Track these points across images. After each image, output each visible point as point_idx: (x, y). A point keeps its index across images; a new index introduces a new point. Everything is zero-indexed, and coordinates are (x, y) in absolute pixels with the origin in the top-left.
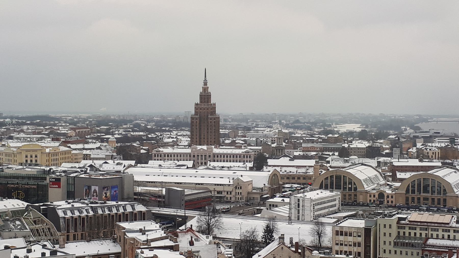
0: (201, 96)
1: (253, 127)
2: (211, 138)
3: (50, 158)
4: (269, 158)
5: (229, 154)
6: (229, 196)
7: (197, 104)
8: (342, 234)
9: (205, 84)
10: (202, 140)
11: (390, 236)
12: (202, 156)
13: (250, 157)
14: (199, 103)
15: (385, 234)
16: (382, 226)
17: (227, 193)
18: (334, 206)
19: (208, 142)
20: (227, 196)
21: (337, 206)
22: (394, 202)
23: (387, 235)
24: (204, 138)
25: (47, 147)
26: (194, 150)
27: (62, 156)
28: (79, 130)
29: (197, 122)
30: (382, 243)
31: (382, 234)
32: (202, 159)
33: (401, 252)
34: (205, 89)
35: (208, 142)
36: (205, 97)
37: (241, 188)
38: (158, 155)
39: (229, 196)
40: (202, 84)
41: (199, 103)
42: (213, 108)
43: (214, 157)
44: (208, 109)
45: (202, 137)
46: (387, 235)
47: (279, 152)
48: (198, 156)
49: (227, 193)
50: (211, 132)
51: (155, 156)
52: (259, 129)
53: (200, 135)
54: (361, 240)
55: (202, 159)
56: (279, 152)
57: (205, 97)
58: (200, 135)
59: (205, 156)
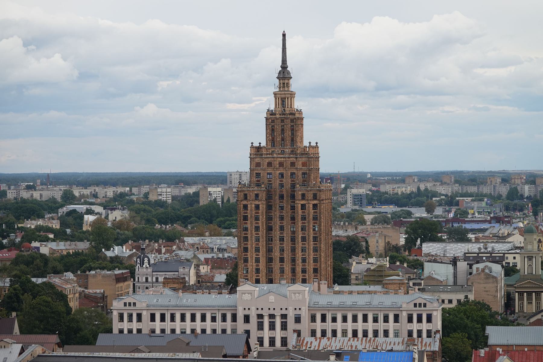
1: (447, 221)
2: (304, 260)
4: (491, 311)
7: (259, 148)
9: (284, 61)
10: (276, 265)
12: (272, 316)
13: (429, 320)
14: (264, 144)
19: (293, 271)
24: (282, 260)
29: (257, 207)
32: (272, 327)
35: (293, 271)
36: (284, 123)
38: (130, 316)
40: (274, 85)
41: (264, 144)
42: (311, 156)
43: (313, 319)
45: (276, 254)
47: (530, 303)
48: (260, 316)
52: (468, 226)
53: (269, 250)
55: (272, 327)
56: (530, 303)
57: (284, 123)
58: (269, 250)
59: (284, 316)
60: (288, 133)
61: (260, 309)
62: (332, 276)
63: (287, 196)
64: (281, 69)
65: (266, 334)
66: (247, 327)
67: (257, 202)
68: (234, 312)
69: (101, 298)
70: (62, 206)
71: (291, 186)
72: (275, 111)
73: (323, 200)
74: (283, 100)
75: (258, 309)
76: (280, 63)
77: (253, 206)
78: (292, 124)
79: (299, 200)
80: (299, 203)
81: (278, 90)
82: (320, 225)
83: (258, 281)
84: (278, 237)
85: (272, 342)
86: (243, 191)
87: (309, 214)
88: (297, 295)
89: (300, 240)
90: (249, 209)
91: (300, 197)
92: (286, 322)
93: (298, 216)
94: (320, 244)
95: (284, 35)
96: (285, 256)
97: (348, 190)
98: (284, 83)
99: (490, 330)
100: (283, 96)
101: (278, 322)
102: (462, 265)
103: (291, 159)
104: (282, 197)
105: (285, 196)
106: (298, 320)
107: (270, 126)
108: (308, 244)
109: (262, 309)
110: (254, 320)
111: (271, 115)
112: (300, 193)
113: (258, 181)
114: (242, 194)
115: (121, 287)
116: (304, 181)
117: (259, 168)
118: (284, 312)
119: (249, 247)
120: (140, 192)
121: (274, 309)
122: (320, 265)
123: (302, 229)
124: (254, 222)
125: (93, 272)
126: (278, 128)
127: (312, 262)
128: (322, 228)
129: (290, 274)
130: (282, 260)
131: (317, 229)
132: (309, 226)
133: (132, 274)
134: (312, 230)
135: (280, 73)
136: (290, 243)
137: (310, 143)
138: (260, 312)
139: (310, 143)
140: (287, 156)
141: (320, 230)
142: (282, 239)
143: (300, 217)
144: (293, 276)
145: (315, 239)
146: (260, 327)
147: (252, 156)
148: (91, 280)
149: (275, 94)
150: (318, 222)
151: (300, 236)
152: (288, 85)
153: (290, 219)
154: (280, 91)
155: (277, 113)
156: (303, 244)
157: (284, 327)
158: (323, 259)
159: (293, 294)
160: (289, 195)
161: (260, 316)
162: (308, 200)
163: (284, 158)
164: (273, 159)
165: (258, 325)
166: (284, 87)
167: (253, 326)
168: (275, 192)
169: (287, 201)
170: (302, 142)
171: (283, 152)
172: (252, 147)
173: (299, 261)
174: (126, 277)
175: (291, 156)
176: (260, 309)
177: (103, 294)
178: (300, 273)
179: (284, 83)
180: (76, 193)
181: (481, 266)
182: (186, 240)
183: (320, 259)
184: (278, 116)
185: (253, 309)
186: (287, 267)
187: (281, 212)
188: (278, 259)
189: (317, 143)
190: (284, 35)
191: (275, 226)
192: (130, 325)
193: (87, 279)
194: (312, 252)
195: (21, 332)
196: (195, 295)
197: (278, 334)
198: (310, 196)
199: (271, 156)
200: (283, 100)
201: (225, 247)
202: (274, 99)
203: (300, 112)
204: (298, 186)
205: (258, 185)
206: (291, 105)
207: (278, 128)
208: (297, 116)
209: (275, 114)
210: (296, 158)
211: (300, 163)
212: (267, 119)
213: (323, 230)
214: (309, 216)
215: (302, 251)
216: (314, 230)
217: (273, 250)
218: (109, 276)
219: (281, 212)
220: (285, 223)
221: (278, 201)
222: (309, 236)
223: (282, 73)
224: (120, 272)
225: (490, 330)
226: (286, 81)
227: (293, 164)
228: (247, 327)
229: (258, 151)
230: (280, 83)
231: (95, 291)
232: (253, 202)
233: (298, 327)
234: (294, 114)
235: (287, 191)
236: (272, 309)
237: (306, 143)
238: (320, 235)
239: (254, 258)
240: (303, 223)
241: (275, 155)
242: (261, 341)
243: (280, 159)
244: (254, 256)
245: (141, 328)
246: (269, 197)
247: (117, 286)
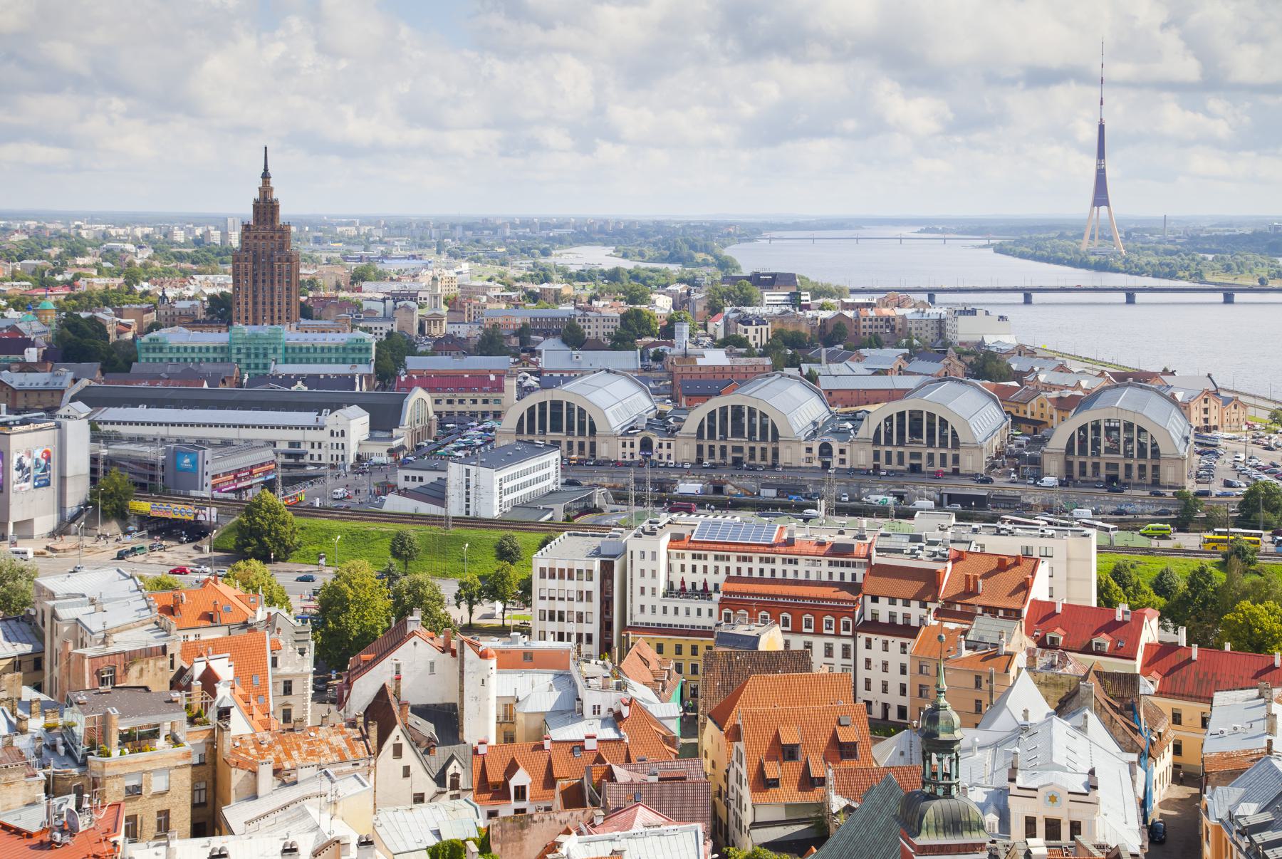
0: (257, 206)
6: (316, 452)
8: (552, 576)
9: (266, 176)
11: (654, 594)
15: (643, 572)
16: (637, 556)
17: (313, 446)
18: (547, 476)
20: (311, 451)
21: (552, 478)
22: (673, 456)
23: (648, 574)
24: (264, 303)
30: (637, 591)
31: (637, 591)
33: (676, 609)
34: (266, 189)
35: (272, 318)
36: (266, 208)
37: (343, 434)
39: (316, 452)
40: (260, 182)
45: (260, 299)
46: (648, 591)
49: (313, 446)
53: (255, 297)
54: (594, 586)
57: (266, 208)
58: (255, 297)
80: (276, 264)
99: (408, 359)
102: (390, 303)
126: (262, 211)
130: (264, 303)
173: (276, 309)
180: (113, 232)
181: (402, 303)
186: (268, 313)
203: (277, 201)
205: (247, 251)
207: (262, 211)
225: (408, 359)
237: (281, 222)
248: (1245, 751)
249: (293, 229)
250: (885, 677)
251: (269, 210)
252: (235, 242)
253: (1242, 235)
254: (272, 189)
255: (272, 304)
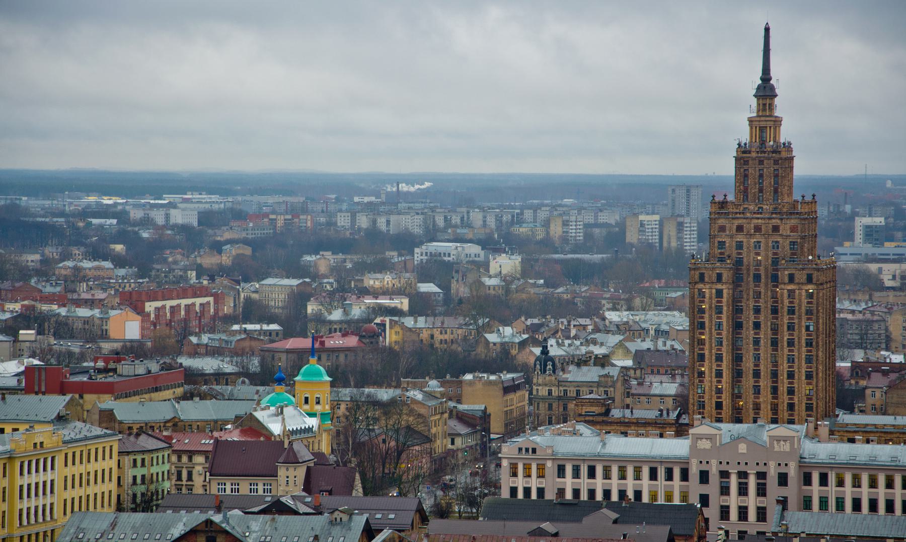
0: (743, 157)
3: (12, 483)
5: (882, 468)
7: (723, 204)
9: (766, 92)
12: (743, 475)
24: (757, 374)
25: (541, 286)
26: (705, 444)
27: (70, 471)
28: (159, 304)
29: (719, 293)
32: (743, 490)
35: (775, 409)
36: (764, 158)
38: (527, 468)
41: (731, 198)
43: (807, 480)
44: (740, 229)
45: (748, 365)
48: (725, 474)
50: (791, 343)
51: (515, 474)
53: (737, 359)
55: (743, 490)
58: (737, 359)
59: (761, 475)
60: (768, 182)
61: (724, 463)
62: (835, 398)
63: (767, 277)
64: (760, 82)
65: (733, 501)
66: (705, 489)
67: (719, 286)
68: (684, 466)
69: (481, 418)
70: (420, 244)
71: (773, 262)
72: (750, 146)
73: (822, 284)
74: (762, 129)
75: (721, 463)
76: (760, 74)
77: (714, 291)
78: (776, 167)
79: (785, 284)
81: (755, 115)
82: (818, 322)
83: (719, 420)
84: (751, 338)
85: (743, 513)
86: (698, 269)
87: (800, 306)
88: (782, 443)
89: (785, 344)
90: (707, 295)
91: (786, 280)
92: (765, 484)
93: (782, 308)
94: (818, 350)
95: (767, 30)
96: (762, 368)
97: (857, 218)
98: (764, 105)
100: (763, 124)
101: (752, 482)
103: (774, 221)
104: (757, 278)
105: (763, 277)
106: (783, 480)
107: (742, 170)
108: (799, 350)
109: (728, 463)
110: (714, 478)
111: (744, 152)
112: (786, 273)
113: (721, 253)
114: (697, 273)
115: (512, 400)
116: (793, 254)
117: (723, 234)
118: (762, 469)
119: (707, 353)
120: (535, 217)
121: (746, 464)
122: (817, 382)
123: (789, 328)
124: (714, 316)
125: (469, 377)
127: (804, 378)
128: (821, 326)
129: (770, 396)
131: (811, 328)
132: (800, 322)
133: (528, 381)
134: (804, 330)
135: (759, 88)
136: (770, 348)
137: (803, 197)
138: (724, 467)
139: (803, 197)
140: (767, 216)
141: (818, 329)
142: (757, 342)
143: (786, 309)
144: (773, 398)
145: (809, 344)
146: (725, 490)
147: (713, 216)
148: (466, 390)
149: (751, 121)
150: (814, 318)
151: (785, 339)
152: (771, 107)
153: (769, 311)
154: (758, 116)
155: (753, 149)
156: (790, 351)
157: (762, 491)
158: (820, 375)
159: (775, 442)
160: (770, 275)
161: (725, 474)
162: (798, 284)
163: (762, 219)
164: (744, 221)
165: (722, 512)
166: (764, 110)
167: (712, 489)
168: (748, 270)
169: (766, 285)
170: (790, 194)
171: (760, 211)
172: (713, 202)
173: (783, 387)
174: (519, 384)
175: (774, 216)
176: (724, 463)
177: (485, 411)
178: (785, 394)
179: (764, 105)
182: (607, 316)
183: (817, 374)
184: (754, 155)
185: (714, 463)
186: (765, 398)
187: (756, 302)
188: (751, 372)
189: (814, 196)
190: (767, 30)
191: (748, 322)
192: (527, 482)
193: (461, 387)
194: (803, 362)
195: (366, 494)
196: (625, 439)
197: (752, 501)
198: (801, 276)
199: (742, 216)
200: (762, 129)
201: (665, 327)
202: (748, 128)
203: (788, 147)
204: (783, 262)
206: (775, 137)
208: (784, 154)
209: (750, 152)
210: (782, 219)
211: (788, 227)
212: (737, 159)
213: (821, 329)
214: (800, 308)
215: (789, 362)
216: (807, 328)
217: (744, 359)
218: (491, 383)
219: (756, 302)
220: (762, 318)
221: (752, 285)
222: (799, 338)
223: (762, 88)
224: (510, 376)
226: (768, 102)
227: (776, 229)
228: (705, 489)
229: (723, 208)
230: (759, 105)
231: (471, 407)
232: (714, 286)
233: (783, 492)
234: (780, 152)
235: (766, 269)
236: (743, 464)
238: (817, 338)
239: (714, 370)
240: (790, 319)
241: (748, 215)
242: (725, 513)
243: (756, 221)
244: (714, 367)
245: (543, 486)
246: (737, 281)
247: (505, 398)
248: (625, 434)
249: (822, 212)
250: (743, 502)
251: (769, 169)
252: (691, 244)
253: (705, 449)
254: (778, 122)
255: (775, 375)
